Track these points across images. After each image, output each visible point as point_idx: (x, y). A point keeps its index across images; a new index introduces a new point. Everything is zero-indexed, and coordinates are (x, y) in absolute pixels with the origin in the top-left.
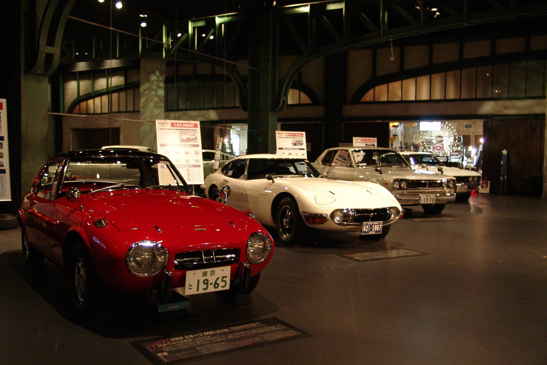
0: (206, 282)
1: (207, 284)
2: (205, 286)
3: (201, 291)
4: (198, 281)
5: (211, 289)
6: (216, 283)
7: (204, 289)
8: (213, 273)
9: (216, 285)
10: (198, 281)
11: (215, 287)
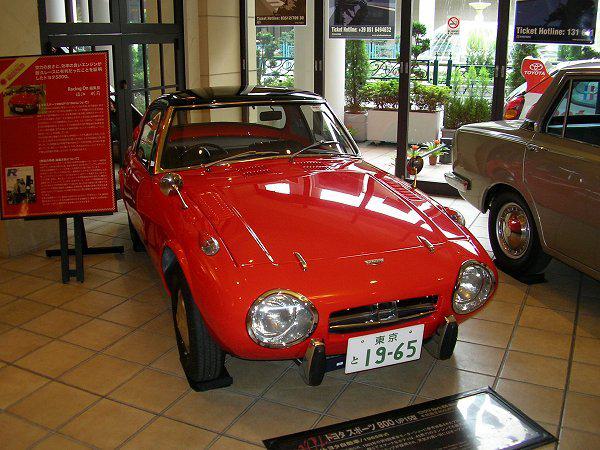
0: (382, 352)
1: (383, 355)
2: (380, 358)
3: (373, 365)
4: (369, 351)
5: (390, 360)
6: (397, 352)
7: (377, 362)
8: (393, 338)
9: (398, 353)
10: (369, 351)
11: (396, 358)
